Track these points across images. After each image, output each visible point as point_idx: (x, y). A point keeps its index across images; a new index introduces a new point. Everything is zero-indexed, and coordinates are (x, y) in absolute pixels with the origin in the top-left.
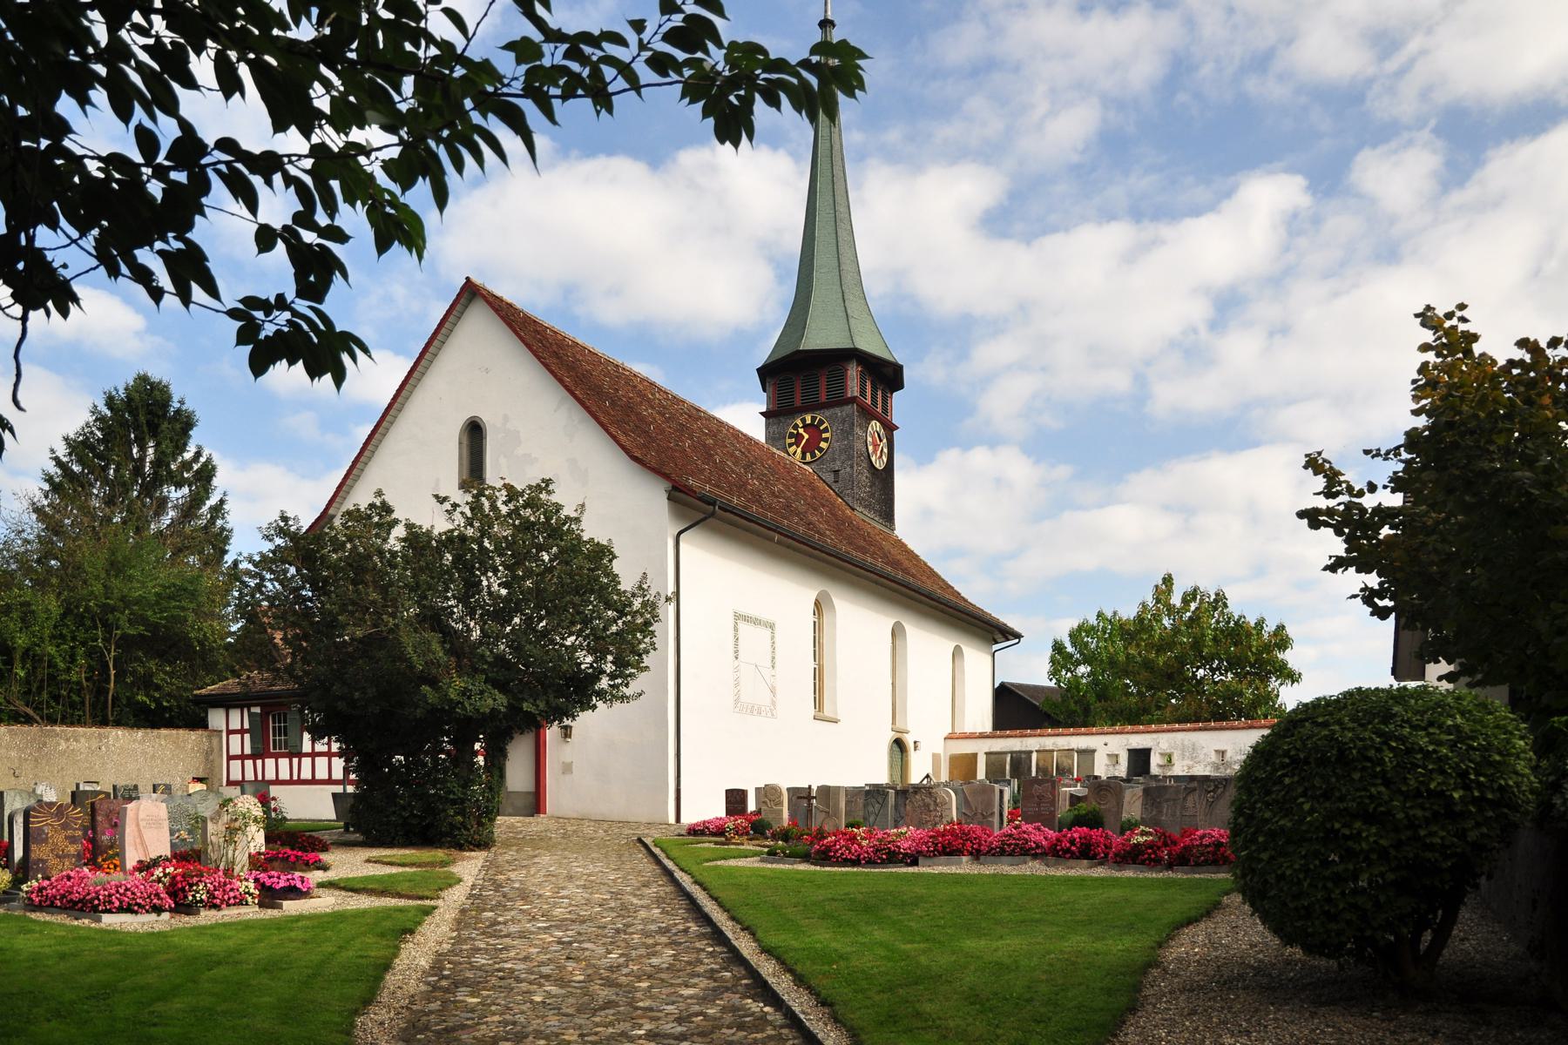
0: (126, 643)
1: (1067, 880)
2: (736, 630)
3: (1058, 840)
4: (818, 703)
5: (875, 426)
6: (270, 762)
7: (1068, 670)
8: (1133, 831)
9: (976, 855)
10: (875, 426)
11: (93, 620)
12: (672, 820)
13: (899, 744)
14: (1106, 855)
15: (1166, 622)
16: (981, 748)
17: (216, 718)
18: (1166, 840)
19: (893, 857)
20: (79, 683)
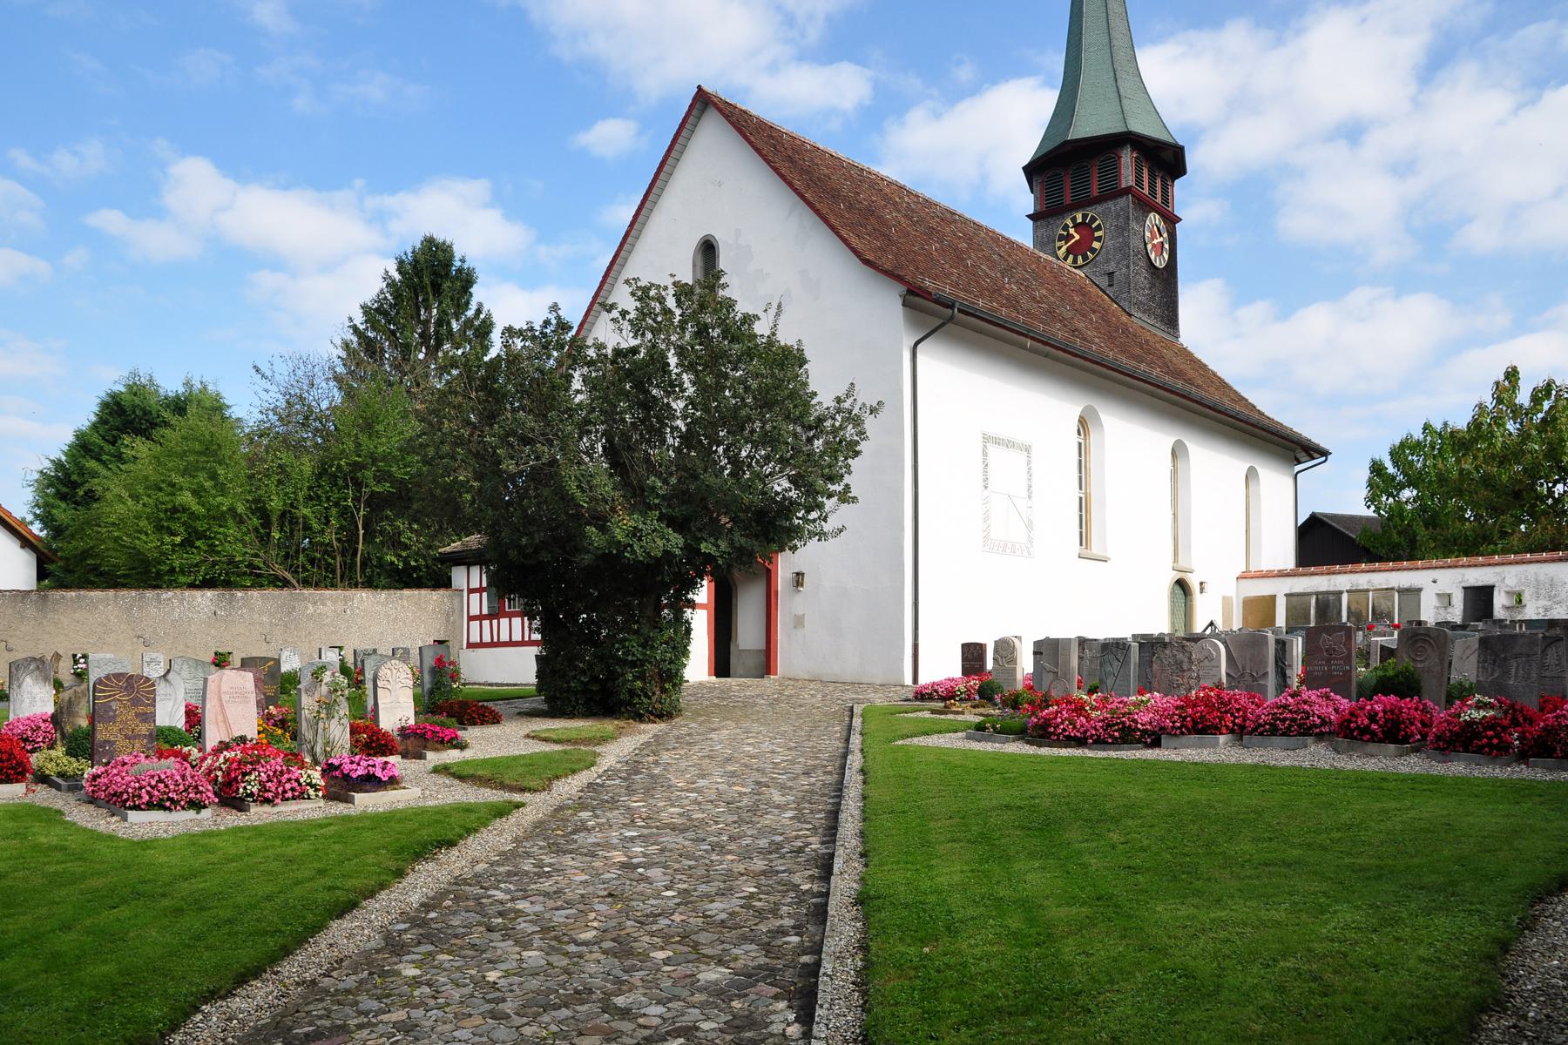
0: (377, 504)
1: (1360, 778)
2: (985, 454)
3: (1352, 714)
4: (1084, 539)
5: (1154, 219)
6: (504, 622)
7: (1390, 495)
8: (1464, 700)
9: (1240, 732)
10: (1154, 219)
11: (345, 480)
12: (908, 680)
13: (1181, 584)
14: (1424, 737)
15: (1511, 426)
16: (1280, 589)
17: (459, 576)
18: (1516, 715)
19: (1127, 735)
20: (330, 544)
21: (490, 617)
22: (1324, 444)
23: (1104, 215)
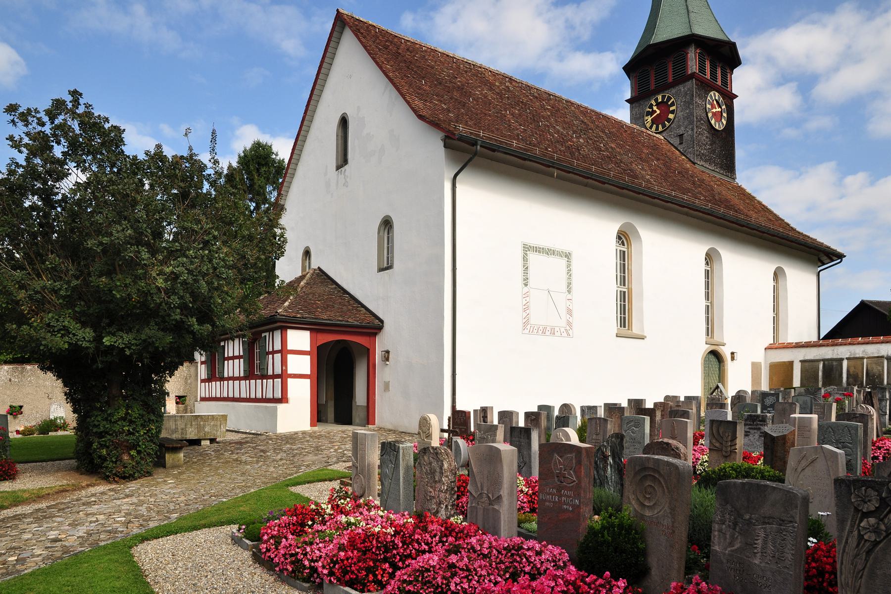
4: (624, 320)
5: (714, 95)
10: (714, 95)
16: (797, 357)
21: (245, 378)
22: (840, 250)
23: (676, 95)
